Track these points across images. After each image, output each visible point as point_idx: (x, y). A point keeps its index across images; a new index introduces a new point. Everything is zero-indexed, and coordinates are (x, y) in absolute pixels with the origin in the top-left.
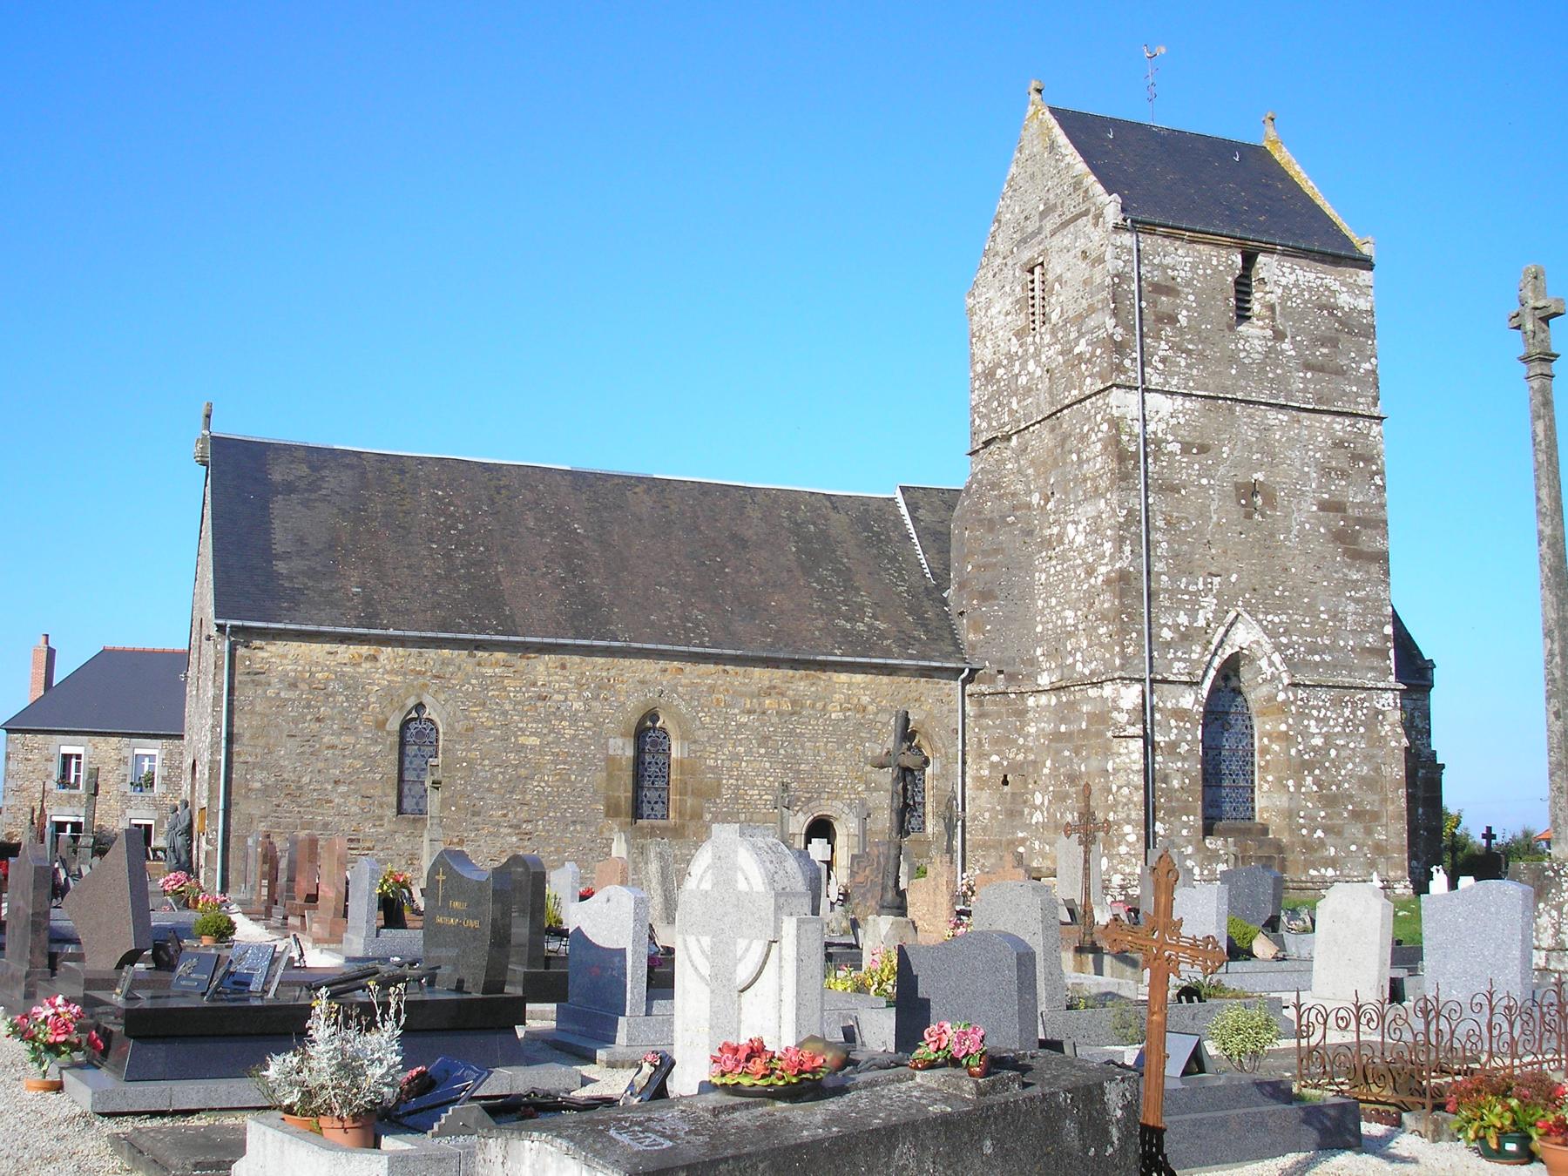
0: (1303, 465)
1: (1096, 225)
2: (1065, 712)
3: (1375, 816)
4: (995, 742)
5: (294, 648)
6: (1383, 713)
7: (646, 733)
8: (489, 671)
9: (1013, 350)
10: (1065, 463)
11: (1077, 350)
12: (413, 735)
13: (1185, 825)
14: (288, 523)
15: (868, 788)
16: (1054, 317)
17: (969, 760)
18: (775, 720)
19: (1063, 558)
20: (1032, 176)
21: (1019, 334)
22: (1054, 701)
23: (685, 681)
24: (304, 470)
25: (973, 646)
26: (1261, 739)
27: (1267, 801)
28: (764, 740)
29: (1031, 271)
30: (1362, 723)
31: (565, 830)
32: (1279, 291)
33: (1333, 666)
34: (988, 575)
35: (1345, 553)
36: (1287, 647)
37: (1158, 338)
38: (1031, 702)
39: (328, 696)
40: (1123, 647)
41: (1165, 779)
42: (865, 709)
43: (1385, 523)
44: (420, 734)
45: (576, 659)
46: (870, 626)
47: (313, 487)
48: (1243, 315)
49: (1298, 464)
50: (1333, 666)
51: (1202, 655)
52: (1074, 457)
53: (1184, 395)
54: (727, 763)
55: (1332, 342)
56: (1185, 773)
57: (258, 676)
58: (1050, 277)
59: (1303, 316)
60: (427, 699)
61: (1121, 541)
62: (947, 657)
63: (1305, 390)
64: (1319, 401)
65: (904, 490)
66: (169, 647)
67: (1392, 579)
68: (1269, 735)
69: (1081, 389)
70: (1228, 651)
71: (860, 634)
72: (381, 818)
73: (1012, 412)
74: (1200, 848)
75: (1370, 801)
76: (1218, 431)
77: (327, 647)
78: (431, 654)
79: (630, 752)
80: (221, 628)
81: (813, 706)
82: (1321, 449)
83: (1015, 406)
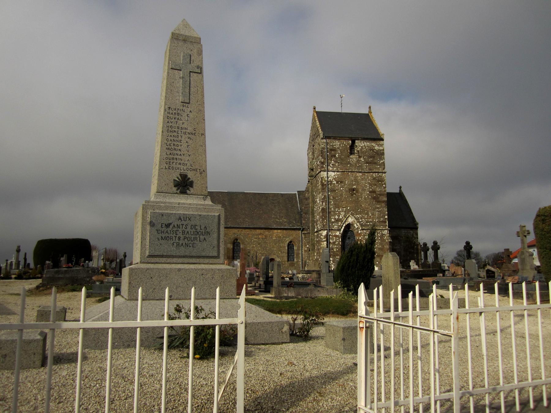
28: (259, 244)
37: (331, 160)
41: (333, 249)
55: (373, 157)
56: (337, 248)
59: (366, 152)
70: (347, 223)
79: (232, 247)
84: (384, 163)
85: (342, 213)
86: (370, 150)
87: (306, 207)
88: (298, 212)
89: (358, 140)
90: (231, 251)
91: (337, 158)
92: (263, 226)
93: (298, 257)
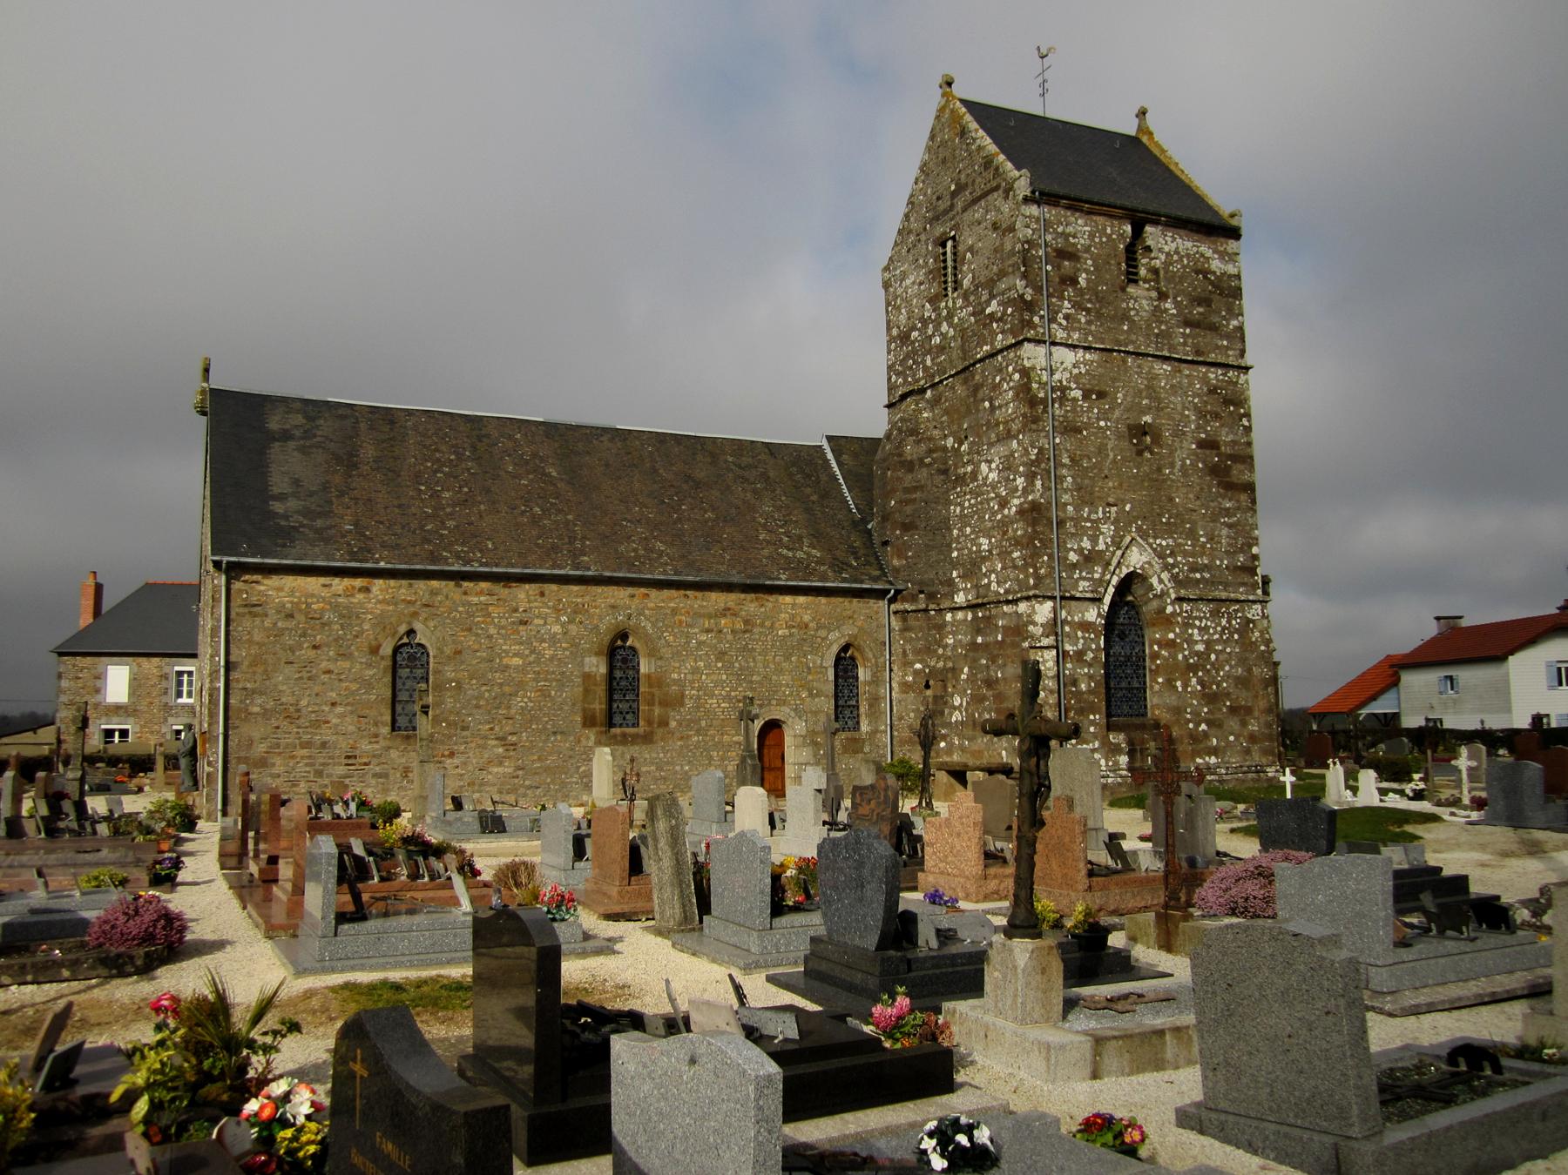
0: (1185, 408)
1: (1006, 198)
2: (977, 627)
3: (1249, 711)
4: (917, 652)
5: (289, 581)
6: (1253, 621)
7: (619, 651)
8: (475, 600)
9: (927, 314)
10: (978, 410)
11: (988, 311)
12: (407, 661)
13: (1093, 723)
14: (288, 468)
15: (811, 695)
16: (966, 283)
17: (895, 668)
18: (730, 637)
19: (976, 493)
20: (944, 161)
21: (934, 300)
22: (970, 617)
23: (651, 605)
24: (299, 419)
25: (896, 570)
26: (1151, 647)
27: (1158, 700)
28: (721, 655)
29: (944, 245)
30: (1237, 631)
31: (545, 741)
32: (1163, 257)
33: (1212, 583)
34: (908, 509)
35: (1219, 485)
36: (1173, 566)
37: (1062, 298)
38: (949, 617)
39: (324, 625)
40: (1036, 569)
41: (1075, 683)
42: (807, 626)
43: (1251, 458)
44: (412, 658)
45: (554, 587)
46: (808, 554)
47: (308, 435)
48: (1132, 278)
49: (1179, 408)
50: (1212, 583)
51: (1103, 574)
52: (987, 404)
53: (1085, 348)
54: (689, 677)
55: (1204, 301)
56: (1091, 677)
57: (255, 608)
58: (961, 248)
59: (1182, 279)
60: (418, 626)
61: (1031, 477)
62: (875, 579)
63: (1185, 344)
64: (1198, 353)
65: (830, 439)
66: (186, 581)
67: (1259, 507)
68: (1159, 643)
69: (992, 344)
70: (1125, 571)
71: (800, 561)
72: (376, 736)
73: (926, 369)
74: (1105, 743)
75: (1244, 697)
76: (1114, 380)
77: (322, 580)
78: (421, 585)
79: (603, 670)
80: (217, 565)
81: (762, 625)
82: (1198, 395)
83: (929, 363)
84: (1240, 329)
85: (1104, 528)
86: (1197, 272)
87: (908, 502)
88: (855, 524)
89: (1155, 223)
90: (601, 691)
91: (1081, 292)
92: (736, 579)
93: (874, 714)
